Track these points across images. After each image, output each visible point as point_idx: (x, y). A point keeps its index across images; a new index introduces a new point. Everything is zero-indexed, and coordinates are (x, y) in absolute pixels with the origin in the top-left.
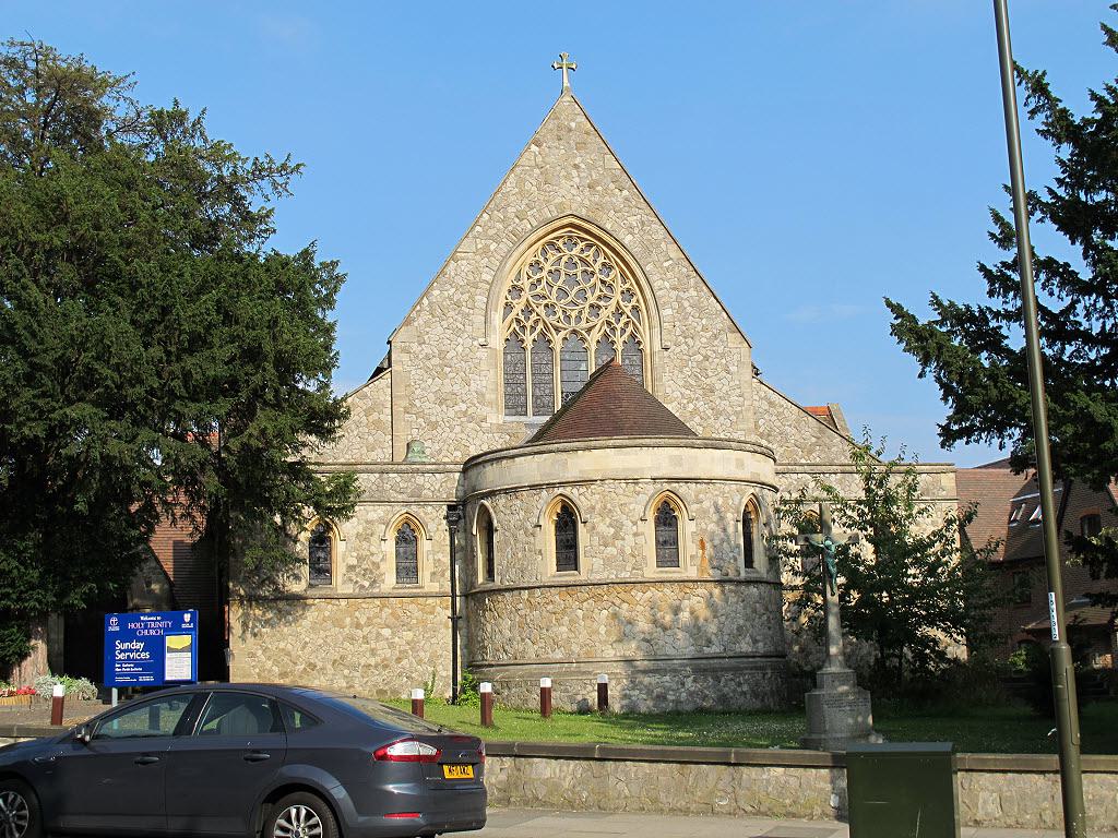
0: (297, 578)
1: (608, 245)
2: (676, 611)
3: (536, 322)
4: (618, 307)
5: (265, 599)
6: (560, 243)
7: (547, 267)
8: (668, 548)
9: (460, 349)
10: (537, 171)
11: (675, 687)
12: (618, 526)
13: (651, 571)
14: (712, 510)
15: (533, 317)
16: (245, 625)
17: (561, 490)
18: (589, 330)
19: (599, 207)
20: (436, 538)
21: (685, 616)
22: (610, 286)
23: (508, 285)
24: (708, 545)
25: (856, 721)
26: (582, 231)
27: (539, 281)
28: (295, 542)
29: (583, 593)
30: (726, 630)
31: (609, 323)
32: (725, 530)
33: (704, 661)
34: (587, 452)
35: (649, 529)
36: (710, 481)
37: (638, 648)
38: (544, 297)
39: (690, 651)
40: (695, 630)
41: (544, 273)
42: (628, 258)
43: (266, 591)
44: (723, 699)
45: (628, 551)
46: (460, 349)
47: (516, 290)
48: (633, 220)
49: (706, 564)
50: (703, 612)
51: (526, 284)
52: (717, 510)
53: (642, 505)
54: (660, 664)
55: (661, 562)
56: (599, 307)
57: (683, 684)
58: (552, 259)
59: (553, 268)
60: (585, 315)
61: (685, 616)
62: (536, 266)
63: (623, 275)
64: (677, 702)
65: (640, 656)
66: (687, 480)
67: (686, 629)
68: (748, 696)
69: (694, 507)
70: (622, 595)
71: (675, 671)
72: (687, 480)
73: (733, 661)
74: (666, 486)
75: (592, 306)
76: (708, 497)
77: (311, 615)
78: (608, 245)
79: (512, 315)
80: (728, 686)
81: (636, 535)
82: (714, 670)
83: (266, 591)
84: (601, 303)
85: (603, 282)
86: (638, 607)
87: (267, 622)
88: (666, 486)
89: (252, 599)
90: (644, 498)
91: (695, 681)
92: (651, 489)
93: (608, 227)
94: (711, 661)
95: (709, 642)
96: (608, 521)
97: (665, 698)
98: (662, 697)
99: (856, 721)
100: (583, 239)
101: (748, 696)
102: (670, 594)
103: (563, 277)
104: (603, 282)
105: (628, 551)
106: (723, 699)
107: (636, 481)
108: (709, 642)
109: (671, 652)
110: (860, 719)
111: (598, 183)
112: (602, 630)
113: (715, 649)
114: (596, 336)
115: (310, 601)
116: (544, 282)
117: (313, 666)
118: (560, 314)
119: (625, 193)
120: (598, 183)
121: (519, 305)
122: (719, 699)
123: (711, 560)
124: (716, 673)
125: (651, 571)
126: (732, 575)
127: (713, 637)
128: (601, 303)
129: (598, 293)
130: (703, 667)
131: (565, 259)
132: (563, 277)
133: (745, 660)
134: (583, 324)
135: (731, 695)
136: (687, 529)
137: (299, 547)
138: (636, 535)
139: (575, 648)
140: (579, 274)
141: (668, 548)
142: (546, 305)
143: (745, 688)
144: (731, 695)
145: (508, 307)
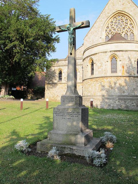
0: (56, 80)
1: (126, 15)
2: (115, 83)
3: (112, 33)
4: (129, 27)
5: (51, 84)
6: (117, 17)
7: (114, 22)
8: (114, 69)
9: (96, 39)
10: (112, 4)
11: (113, 103)
12: (101, 63)
13: (109, 74)
14: (127, 58)
15: (111, 32)
16: (47, 88)
17: (90, 57)
18: (123, 33)
19: (125, 8)
20: (80, 72)
21: (118, 85)
22: (127, 23)
23: (106, 26)
24: (125, 67)
25: (72, 125)
26: (121, 14)
27: (112, 25)
28: (56, 73)
29: (94, 80)
30: (130, 89)
31: (127, 31)
32: (131, 63)
33: (122, 97)
34: (96, 47)
35: (109, 64)
36: (126, 51)
37: (105, 93)
38: (113, 28)
39: (119, 94)
40: (120, 88)
41: (114, 23)
42: (130, 17)
43: (51, 82)
44: (127, 107)
45: (104, 69)
46: (96, 39)
47: (108, 27)
48: (132, 9)
49: (125, 72)
50: (124, 84)
51: (110, 26)
52: (129, 58)
53: (107, 57)
54: (110, 97)
55: (112, 72)
56: (125, 28)
57: (115, 102)
58: (115, 20)
59: (115, 22)
60: (122, 29)
61: (118, 85)
62: (112, 22)
63: (130, 21)
64: (113, 107)
65: (105, 94)
66: (119, 51)
67: (118, 88)
68: (135, 107)
69: (121, 58)
70: (102, 80)
71: (114, 99)
72: (119, 51)
73: (131, 97)
74: (113, 53)
75: (123, 28)
76: (125, 55)
77: (58, 86)
78: (126, 15)
79: (107, 32)
80: (129, 103)
81: (106, 65)
82: (125, 99)
83: (51, 82)
84: (125, 27)
85: (126, 23)
86: (106, 83)
87: (51, 88)
88: (113, 53)
89: (49, 84)
90: (108, 56)
91: (119, 102)
92: (110, 54)
93: (126, 11)
94: (124, 97)
95: (124, 92)
96: (99, 62)
97: (110, 106)
98: (109, 105)
99: (72, 125)
100: (121, 15)
101: (135, 107)
102: (113, 80)
103: (117, 23)
104: (126, 23)
105: (104, 69)
106: (127, 107)
107: (106, 52)
108: (124, 92)
109: (113, 94)
110: (75, 123)
111: (124, 3)
112: (97, 88)
113: (126, 94)
114: (124, 33)
115: (58, 84)
116: (113, 25)
117: (58, 96)
118: (116, 30)
119: (130, 4)
120: (124, 3)
121: (108, 30)
122: (125, 107)
123: (126, 71)
124: (125, 99)
125: (109, 74)
126: (133, 75)
127: (125, 91)
128: (125, 27)
129: (124, 25)
130: (121, 98)
131: (118, 20)
132: (117, 23)
133: (135, 97)
134: (121, 32)
135: (130, 106)
136: (119, 64)
137: (56, 74)
138: (106, 65)
139: (92, 93)
140: (121, 22)
141: (114, 69)
142: (114, 29)
143: (134, 104)
144: (130, 106)
145: (106, 30)
